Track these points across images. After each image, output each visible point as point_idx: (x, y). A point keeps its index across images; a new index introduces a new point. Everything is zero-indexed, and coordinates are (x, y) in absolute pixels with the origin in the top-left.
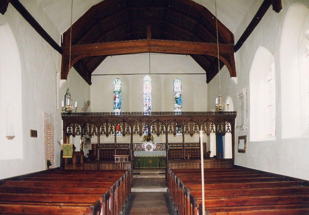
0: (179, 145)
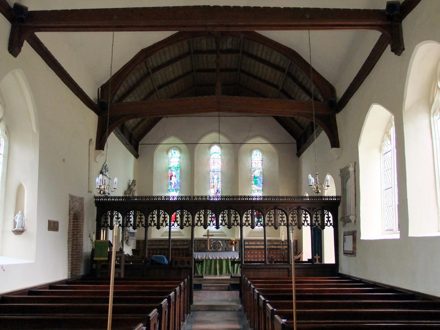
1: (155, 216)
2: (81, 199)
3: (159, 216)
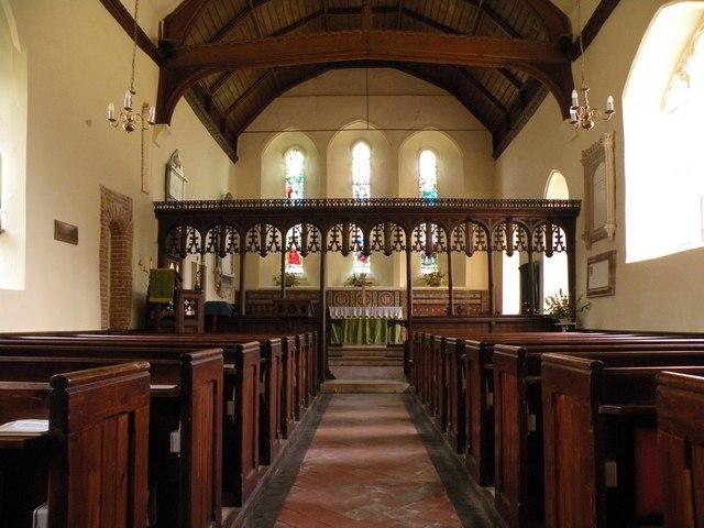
0: (431, 296)
1: (258, 234)
2: (126, 201)
3: (264, 234)
